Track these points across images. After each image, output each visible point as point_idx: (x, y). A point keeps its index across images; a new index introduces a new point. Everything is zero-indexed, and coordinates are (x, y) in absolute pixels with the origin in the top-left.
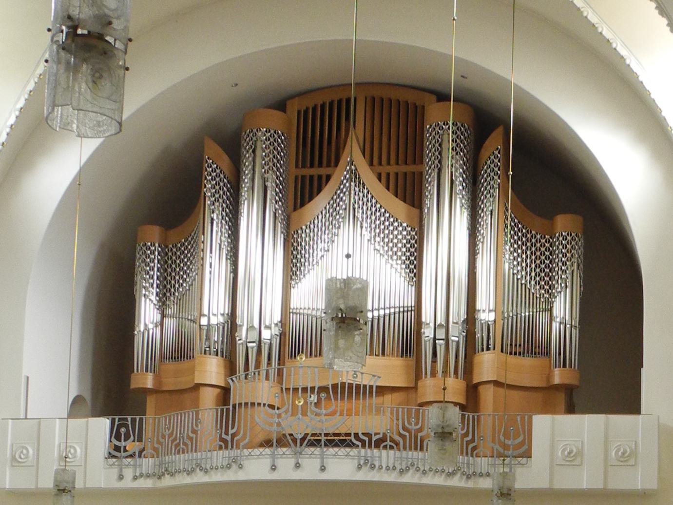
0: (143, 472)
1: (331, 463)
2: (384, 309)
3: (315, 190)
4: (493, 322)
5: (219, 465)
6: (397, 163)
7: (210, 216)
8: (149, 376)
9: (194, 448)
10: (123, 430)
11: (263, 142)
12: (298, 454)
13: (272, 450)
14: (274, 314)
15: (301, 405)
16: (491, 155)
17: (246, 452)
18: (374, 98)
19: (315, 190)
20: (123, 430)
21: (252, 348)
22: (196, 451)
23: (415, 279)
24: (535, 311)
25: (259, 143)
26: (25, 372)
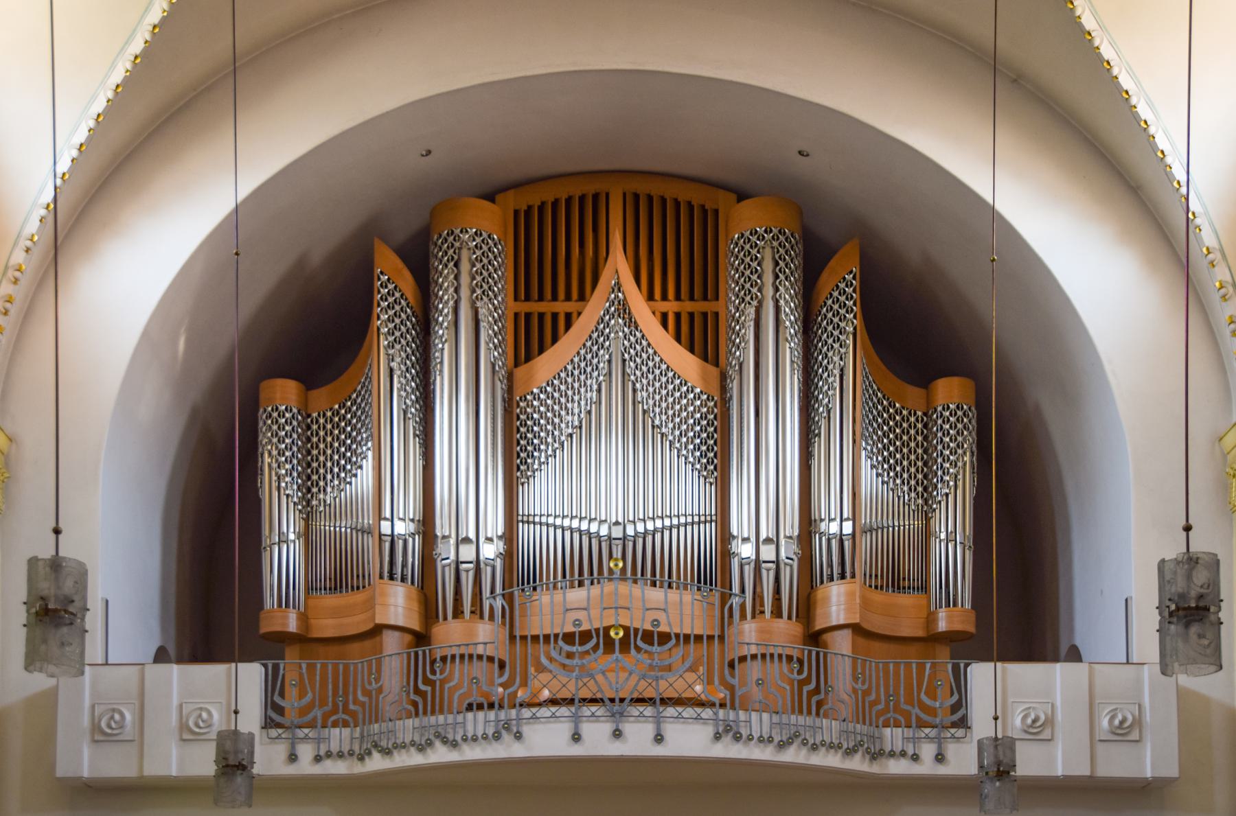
0: (332, 750)
1: (672, 731)
2: (678, 516)
4: (850, 537)
5: (480, 734)
8: (291, 615)
9: (429, 708)
11: (472, 251)
12: (617, 716)
13: (573, 709)
15: (620, 639)
16: (833, 290)
21: (467, 571)
23: (715, 474)
24: (907, 523)
25: (465, 253)
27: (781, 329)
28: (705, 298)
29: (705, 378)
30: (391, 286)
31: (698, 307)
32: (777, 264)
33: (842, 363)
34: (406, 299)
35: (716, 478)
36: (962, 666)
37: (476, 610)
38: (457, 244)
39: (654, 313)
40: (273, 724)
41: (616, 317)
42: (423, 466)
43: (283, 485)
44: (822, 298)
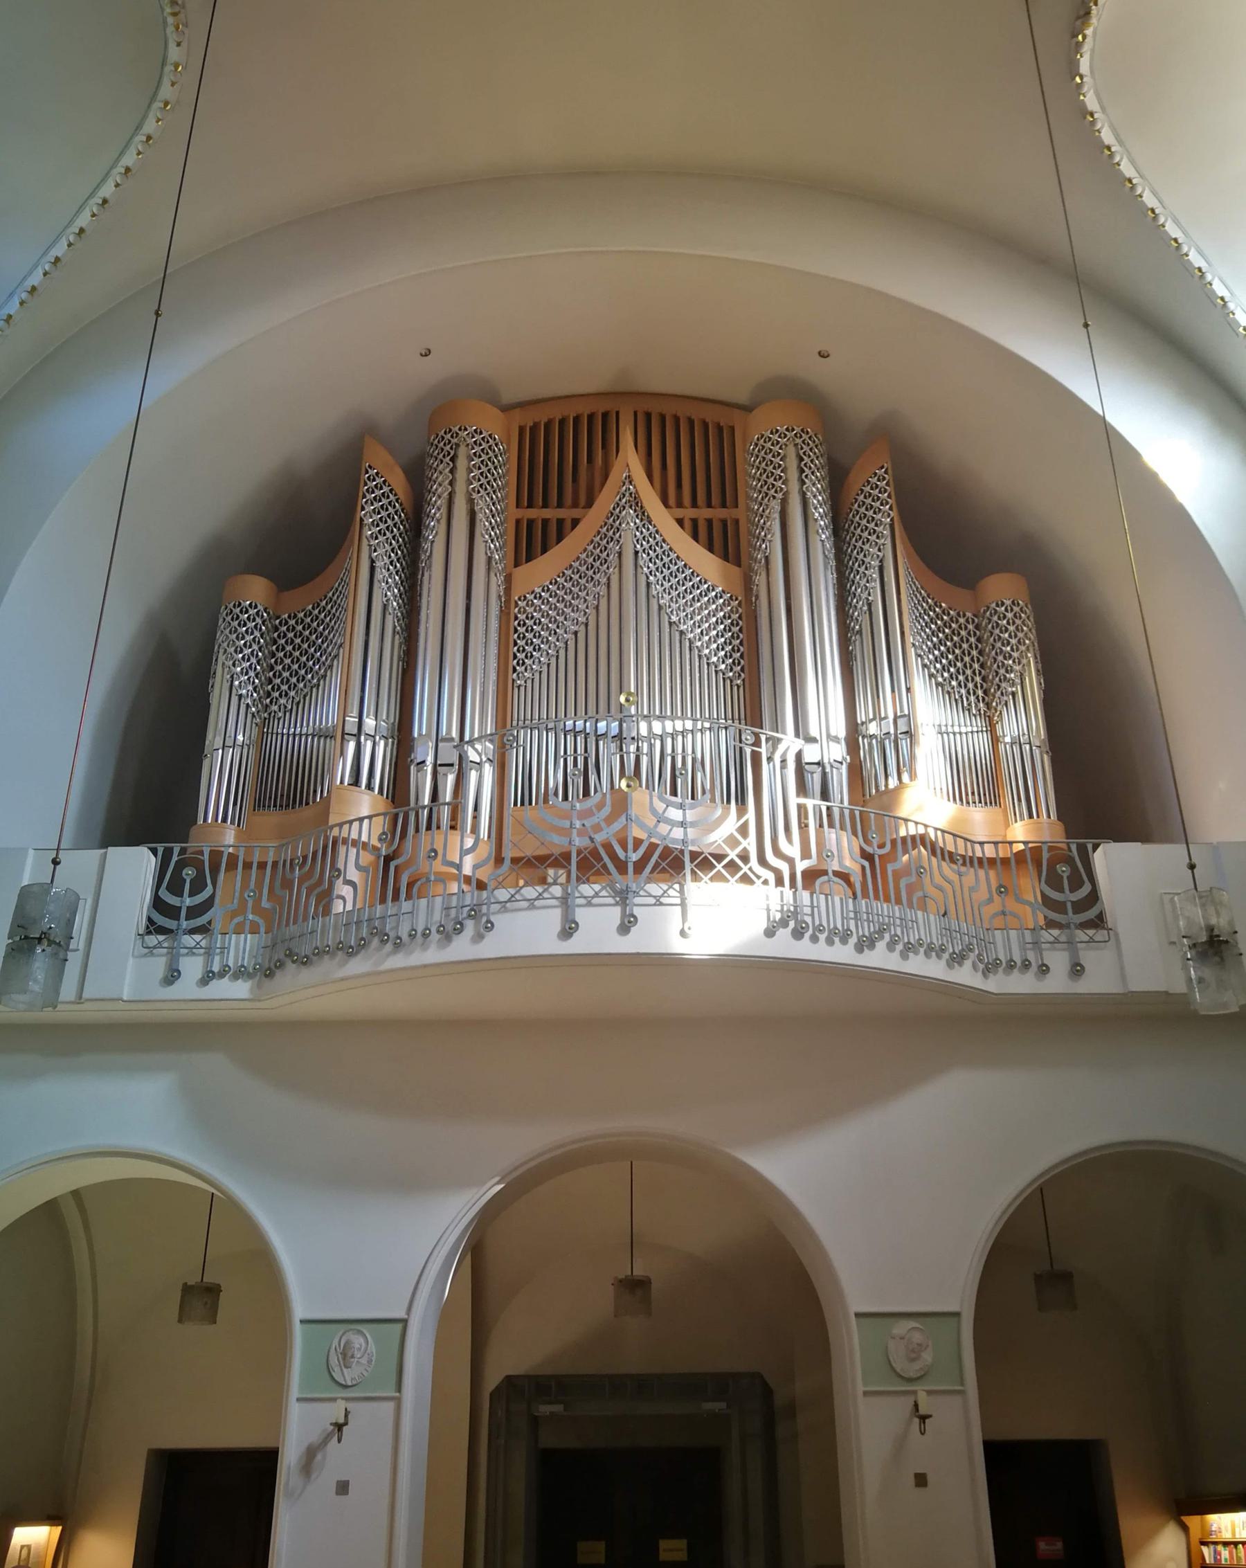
6: (694, 504)
7: (370, 557)
10: (189, 873)
20: (189, 873)
25: (462, 451)
27: (811, 523)
28: (724, 505)
31: (718, 513)
32: (801, 459)
33: (881, 554)
34: (395, 495)
35: (743, 680)
36: (1090, 847)
37: (457, 824)
38: (454, 441)
40: (152, 928)
41: (627, 508)
42: (403, 669)
43: (237, 683)
44: (853, 494)
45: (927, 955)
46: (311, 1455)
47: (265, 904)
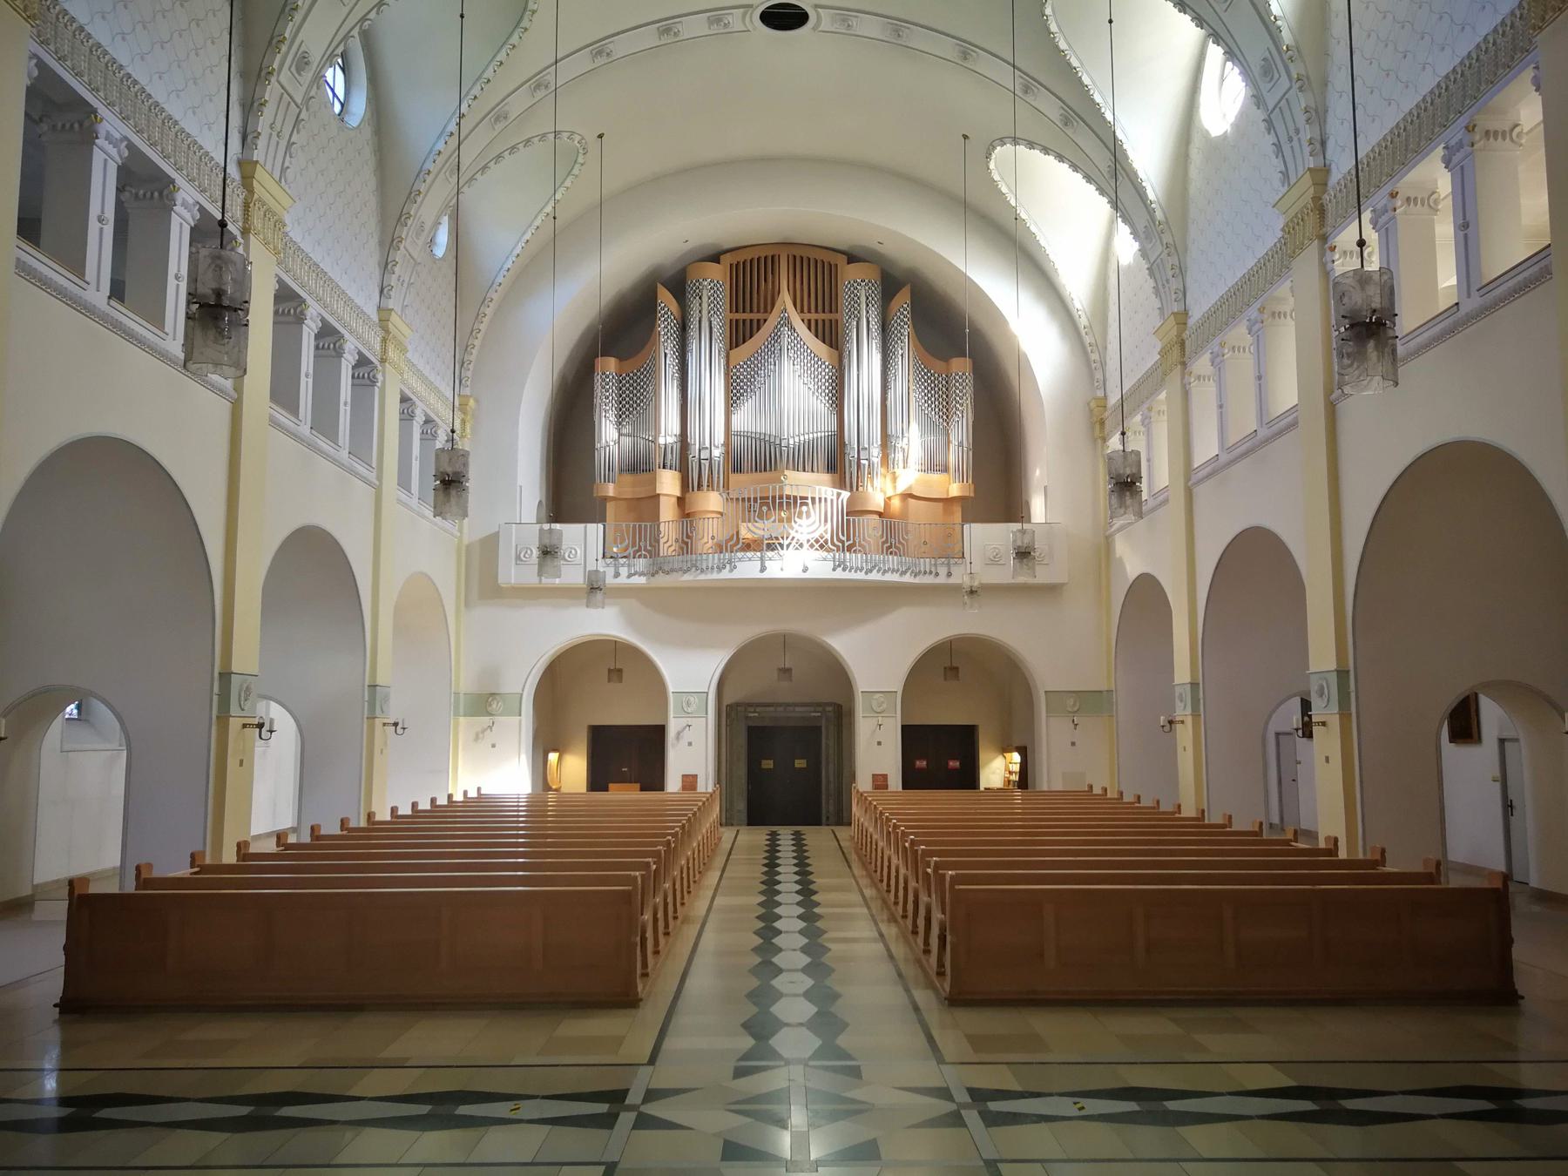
3: (748, 334)
6: (816, 311)
14: (720, 437)
17: (740, 555)
18: (795, 257)
19: (748, 334)
22: (691, 554)
25: (705, 292)
26: (519, 483)
28: (831, 312)
29: (831, 357)
30: (666, 309)
31: (826, 316)
39: (803, 320)
45: (892, 573)
46: (679, 734)
47: (649, 548)
